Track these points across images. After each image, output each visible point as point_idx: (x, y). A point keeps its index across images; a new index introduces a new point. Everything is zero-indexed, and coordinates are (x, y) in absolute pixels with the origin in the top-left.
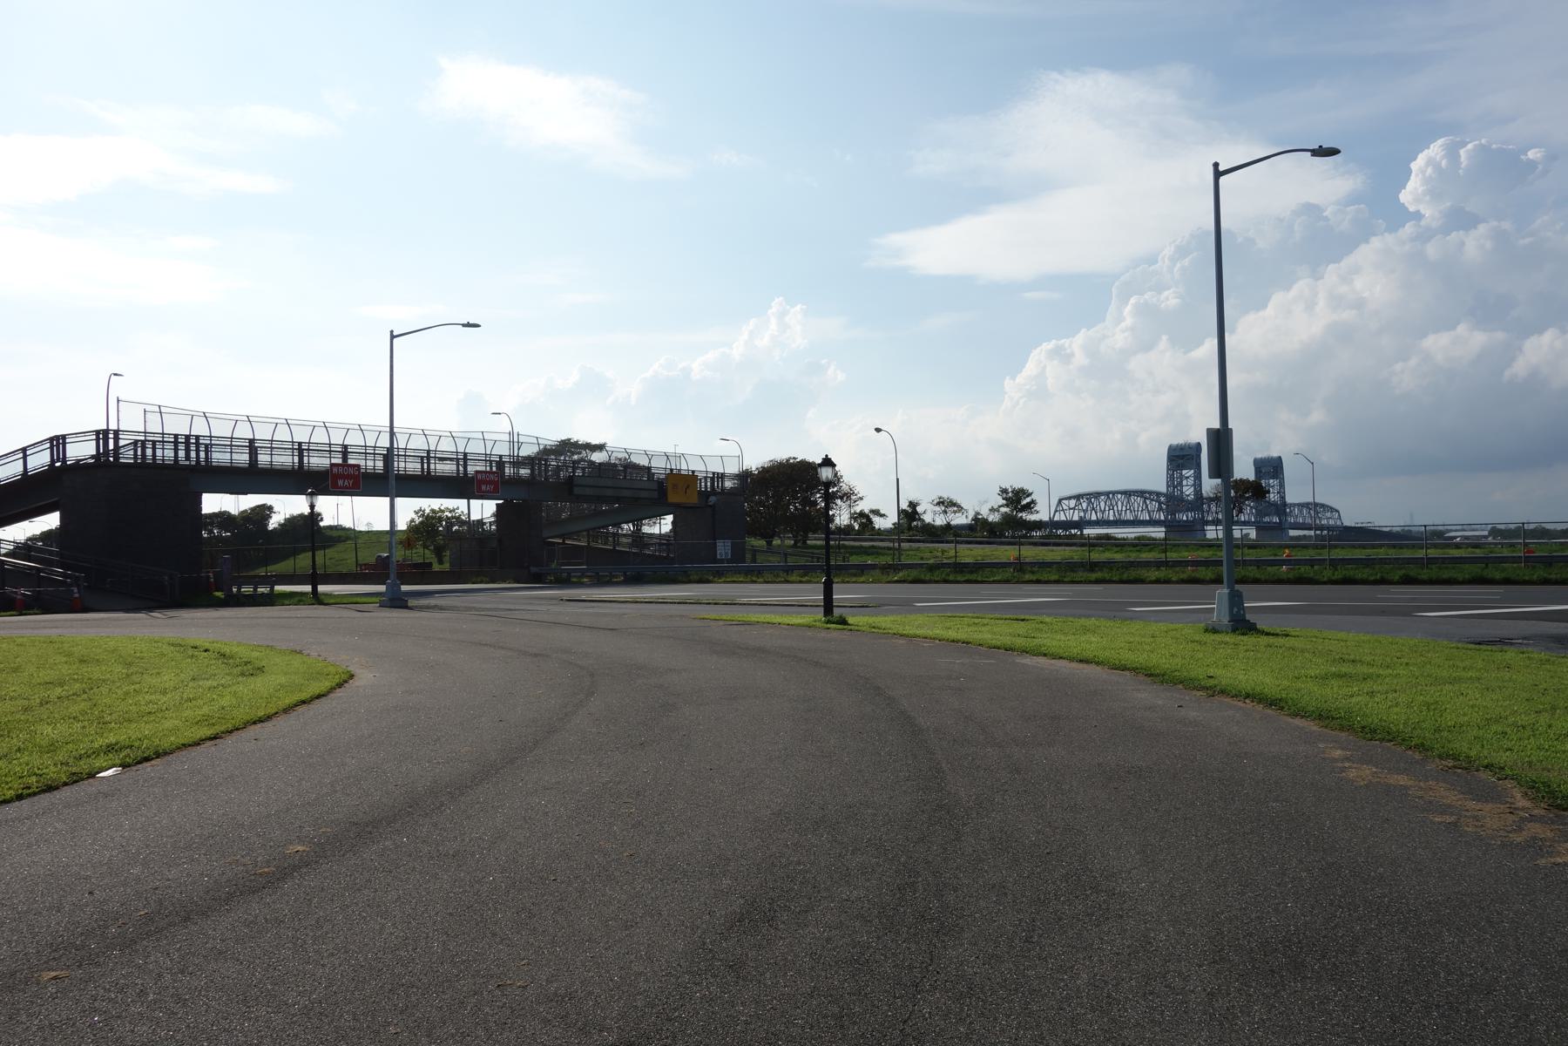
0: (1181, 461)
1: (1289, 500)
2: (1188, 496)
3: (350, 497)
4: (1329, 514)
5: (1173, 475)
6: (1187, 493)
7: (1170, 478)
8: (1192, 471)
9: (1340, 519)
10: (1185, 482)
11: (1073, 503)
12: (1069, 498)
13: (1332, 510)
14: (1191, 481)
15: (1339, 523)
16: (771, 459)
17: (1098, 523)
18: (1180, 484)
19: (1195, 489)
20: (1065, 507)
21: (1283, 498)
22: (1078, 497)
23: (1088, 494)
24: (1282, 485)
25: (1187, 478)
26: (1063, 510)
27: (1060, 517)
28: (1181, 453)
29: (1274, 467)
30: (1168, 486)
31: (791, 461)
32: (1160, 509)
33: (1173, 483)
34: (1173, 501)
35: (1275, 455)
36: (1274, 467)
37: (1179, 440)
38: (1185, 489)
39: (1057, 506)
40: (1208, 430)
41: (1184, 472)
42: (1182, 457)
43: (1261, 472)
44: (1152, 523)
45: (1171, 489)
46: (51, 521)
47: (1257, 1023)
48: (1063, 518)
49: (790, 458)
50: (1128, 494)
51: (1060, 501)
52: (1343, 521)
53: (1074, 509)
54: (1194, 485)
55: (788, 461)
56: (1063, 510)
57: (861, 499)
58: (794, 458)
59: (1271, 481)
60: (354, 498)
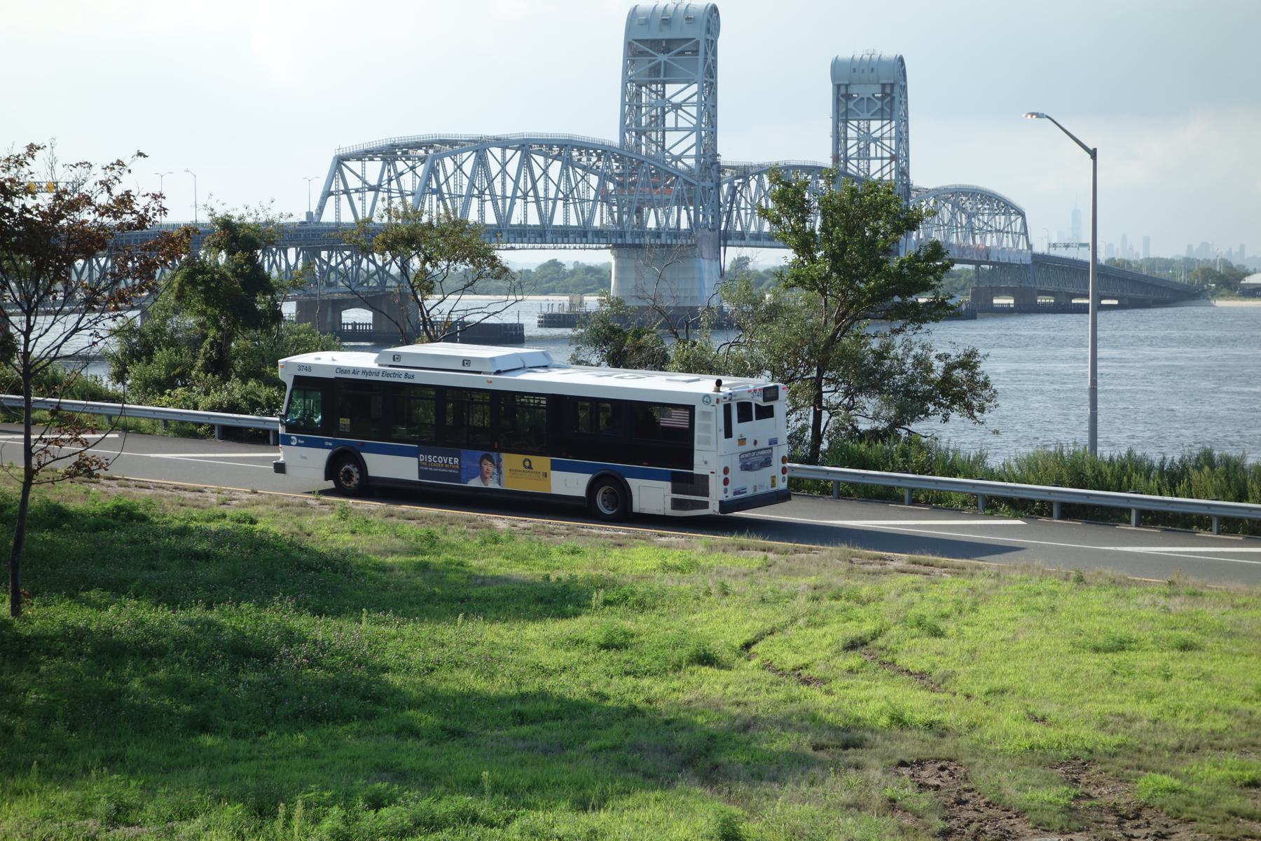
0: (662, 58)
1: (730, 152)
2: (678, 158)
4: (1000, 221)
5: (638, 95)
6: (676, 151)
7: (631, 104)
8: (694, 88)
9: (1026, 233)
10: (670, 119)
11: (373, 170)
12: (364, 155)
13: (1008, 208)
14: (688, 117)
15: (1022, 245)
17: (543, 234)
18: (658, 122)
19: (700, 138)
20: (354, 183)
21: (903, 173)
22: (389, 153)
23: (429, 145)
24: (902, 138)
25: (677, 107)
26: (347, 192)
27: (339, 213)
28: (667, 34)
29: (884, 86)
30: (624, 129)
32: (603, 196)
33: (638, 123)
35: (889, 53)
36: (884, 86)
38: (671, 138)
39: (332, 177)
40: (633, 14)
41: (671, 89)
42: (666, 46)
43: (848, 97)
44: (582, 235)
45: (631, 138)
46: (996, 301)
47: (60, 211)
48: (347, 218)
50: (526, 147)
51: (340, 161)
52: (1032, 241)
53: (376, 189)
54: (696, 129)
56: (347, 192)
59: (875, 125)
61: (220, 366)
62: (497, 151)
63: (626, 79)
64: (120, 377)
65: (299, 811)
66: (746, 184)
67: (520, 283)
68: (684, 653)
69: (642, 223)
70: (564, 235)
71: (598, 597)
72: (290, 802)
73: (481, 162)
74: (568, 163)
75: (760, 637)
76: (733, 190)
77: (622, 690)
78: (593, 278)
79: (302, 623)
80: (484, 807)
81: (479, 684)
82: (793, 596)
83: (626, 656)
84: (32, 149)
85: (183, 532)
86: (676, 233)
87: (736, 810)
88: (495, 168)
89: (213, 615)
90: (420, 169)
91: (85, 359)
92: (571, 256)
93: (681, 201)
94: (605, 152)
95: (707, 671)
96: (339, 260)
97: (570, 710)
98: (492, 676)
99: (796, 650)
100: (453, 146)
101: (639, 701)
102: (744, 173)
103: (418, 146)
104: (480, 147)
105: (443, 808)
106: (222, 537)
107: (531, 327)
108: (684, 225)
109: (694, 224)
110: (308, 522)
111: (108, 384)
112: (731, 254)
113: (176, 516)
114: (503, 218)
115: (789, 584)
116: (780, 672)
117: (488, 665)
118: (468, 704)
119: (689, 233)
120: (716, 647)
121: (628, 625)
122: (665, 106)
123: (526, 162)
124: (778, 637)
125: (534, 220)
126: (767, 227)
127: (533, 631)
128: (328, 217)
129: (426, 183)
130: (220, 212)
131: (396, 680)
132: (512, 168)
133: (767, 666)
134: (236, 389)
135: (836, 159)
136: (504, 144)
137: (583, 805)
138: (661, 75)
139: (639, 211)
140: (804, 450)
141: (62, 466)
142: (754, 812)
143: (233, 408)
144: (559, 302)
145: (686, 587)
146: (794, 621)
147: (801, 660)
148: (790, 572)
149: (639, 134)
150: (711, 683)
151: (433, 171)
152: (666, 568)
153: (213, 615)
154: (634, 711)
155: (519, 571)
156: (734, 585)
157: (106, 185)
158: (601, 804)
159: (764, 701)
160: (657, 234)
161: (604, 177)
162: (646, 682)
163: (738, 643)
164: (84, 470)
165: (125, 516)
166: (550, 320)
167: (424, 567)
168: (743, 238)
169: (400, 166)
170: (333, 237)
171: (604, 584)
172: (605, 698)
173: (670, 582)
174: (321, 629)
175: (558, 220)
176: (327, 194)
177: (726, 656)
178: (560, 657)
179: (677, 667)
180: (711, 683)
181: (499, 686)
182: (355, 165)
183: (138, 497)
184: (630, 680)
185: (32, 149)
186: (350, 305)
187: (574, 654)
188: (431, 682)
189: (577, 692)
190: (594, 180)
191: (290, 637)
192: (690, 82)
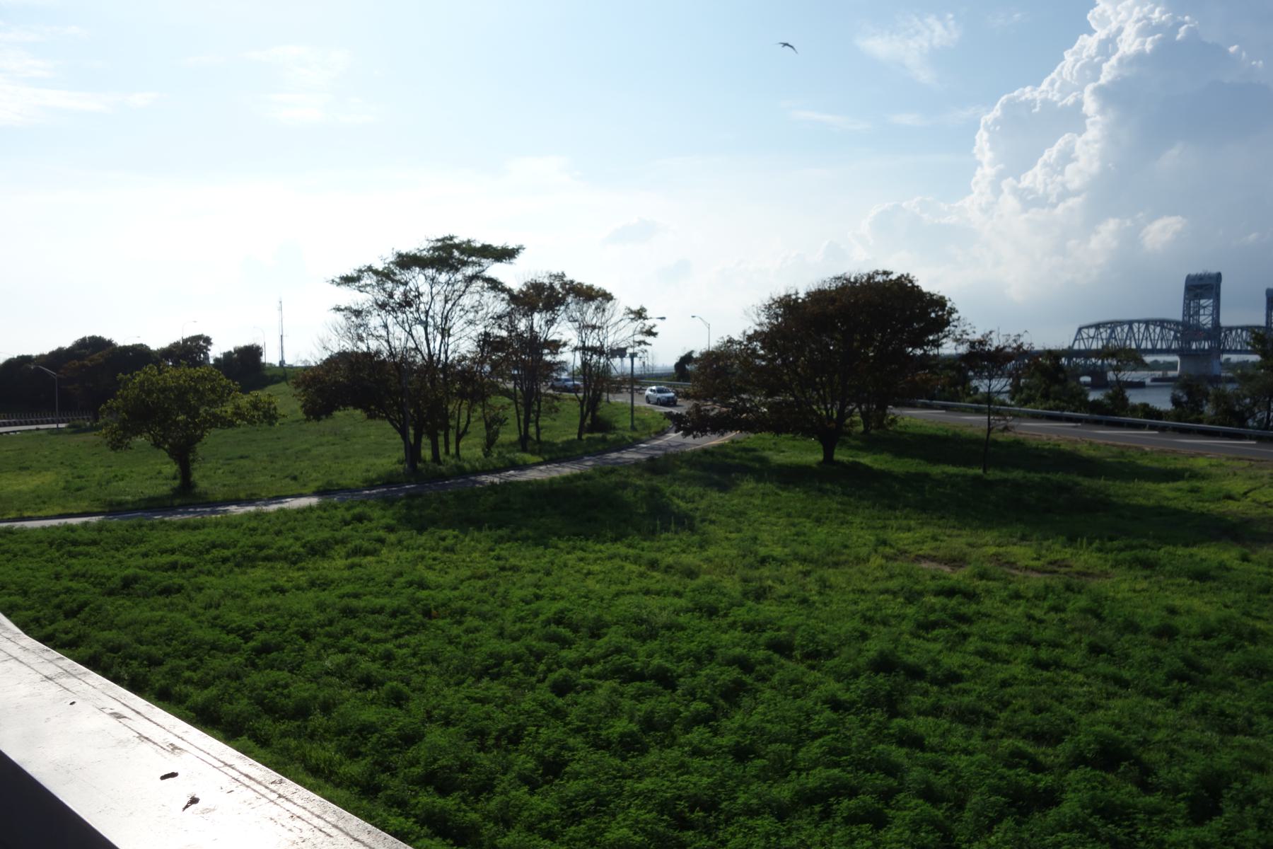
0: (1198, 291)
1: (1225, 321)
3: (289, 361)
7: (1187, 307)
10: (1202, 312)
11: (1092, 332)
12: (1088, 327)
14: (1209, 310)
16: (839, 274)
17: (1154, 351)
18: (1197, 313)
20: (1085, 336)
22: (1097, 326)
23: (1111, 323)
25: (1204, 307)
30: (1184, 315)
31: (879, 279)
32: (1175, 338)
34: (1187, 330)
37: (1197, 269)
38: (1202, 318)
41: (1202, 302)
42: (1201, 287)
44: (1168, 351)
45: (1186, 318)
48: (1082, 347)
49: (877, 273)
50: (1147, 323)
51: (1080, 330)
53: (1093, 338)
54: (1212, 315)
55: (870, 277)
57: (338, 309)
58: (885, 273)
60: (326, 356)
61: (1046, 396)
62: (1136, 325)
63: (1185, 299)
64: (1012, 399)
65: (1085, 540)
66: (1231, 333)
67: (1146, 366)
68: (1221, 495)
69: (1190, 347)
70: (1161, 352)
71: (1187, 474)
72: (1082, 538)
73: (1131, 328)
74: (1163, 328)
75: (1250, 491)
76: (1226, 335)
77: (1197, 506)
78: (1172, 366)
79: (1080, 479)
80: (1150, 543)
81: (1144, 502)
82: (1262, 477)
83: (1198, 495)
84: (991, 332)
85: (1037, 448)
86: (1204, 350)
87: (1247, 551)
88: (1135, 330)
89: (1048, 476)
90: (1109, 331)
91: (999, 392)
92: (1162, 358)
93: (1206, 339)
94: (1177, 323)
95: (1230, 502)
96: (1081, 361)
97: (1176, 512)
98: (1149, 499)
99: (1265, 496)
100: (1121, 323)
101: (1205, 510)
102: (1231, 329)
103: (1107, 323)
104: (1130, 323)
105: (1135, 543)
106: (1049, 450)
107: (1148, 381)
108: (1206, 347)
109: (1210, 347)
110: (1079, 446)
111: (1008, 401)
112: (1225, 357)
113: (1034, 444)
114: (1138, 346)
115: (1260, 473)
116: (1260, 503)
117: (1147, 495)
118: (1141, 509)
119: (1208, 350)
120: (1233, 492)
121: (1198, 484)
122: (1199, 307)
123: (1147, 328)
124: (1257, 491)
125: (1150, 346)
126: (1249, 348)
127: (1163, 485)
128: (1076, 347)
129: (1111, 334)
130: (528, 279)
131: (1115, 499)
132: (1142, 330)
133: (1254, 501)
134: (1051, 403)
135: (1267, 323)
136: (1139, 322)
137: (1186, 545)
138: (1199, 296)
139: (1189, 343)
140: (1263, 426)
141: (1001, 427)
142: (1254, 552)
143: (1050, 409)
144: (1158, 374)
145: (1219, 472)
146: (1264, 485)
147: (1268, 499)
148: (1261, 468)
149: (1190, 316)
150: (1232, 506)
151: (1113, 331)
152: (1211, 466)
153: (1048, 476)
154: (1203, 514)
155: (1155, 465)
156: (1239, 472)
157: (1015, 341)
158: (1194, 544)
159: (1255, 512)
160: (1196, 350)
161: (1176, 332)
162: (1207, 504)
163: (1242, 492)
164: (1006, 429)
165: (1018, 443)
166: (1154, 380)
167: (1120, 463)
168: (1230, 351)
169: (1101, 330)
170: (1079, 353)
171: (1186, 470)
172: (1191, 509)
173: (1213, 470)
174: (1086, 482)
175: (1159, 346)
176: (1075, 340)
177: (1237, 497)
178: (1171, 495)
179: (1219, 500)
180: (1232, 506)
181: (1152, 502)
182: (1086, 330)
183: (1021, 437)
184: (1201, 504)
185: (991, 332)
186: (1083, 375)
187: (1179, 494)
188: (1127, 501)
189: (1180, 506)
190: (1172, 333)
191: (1076, 484)
192: (1209, 298)
